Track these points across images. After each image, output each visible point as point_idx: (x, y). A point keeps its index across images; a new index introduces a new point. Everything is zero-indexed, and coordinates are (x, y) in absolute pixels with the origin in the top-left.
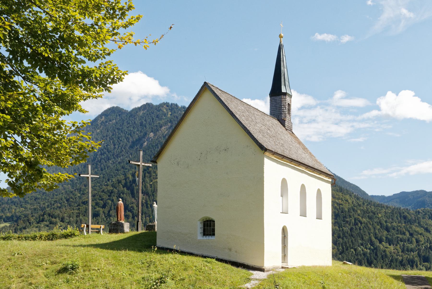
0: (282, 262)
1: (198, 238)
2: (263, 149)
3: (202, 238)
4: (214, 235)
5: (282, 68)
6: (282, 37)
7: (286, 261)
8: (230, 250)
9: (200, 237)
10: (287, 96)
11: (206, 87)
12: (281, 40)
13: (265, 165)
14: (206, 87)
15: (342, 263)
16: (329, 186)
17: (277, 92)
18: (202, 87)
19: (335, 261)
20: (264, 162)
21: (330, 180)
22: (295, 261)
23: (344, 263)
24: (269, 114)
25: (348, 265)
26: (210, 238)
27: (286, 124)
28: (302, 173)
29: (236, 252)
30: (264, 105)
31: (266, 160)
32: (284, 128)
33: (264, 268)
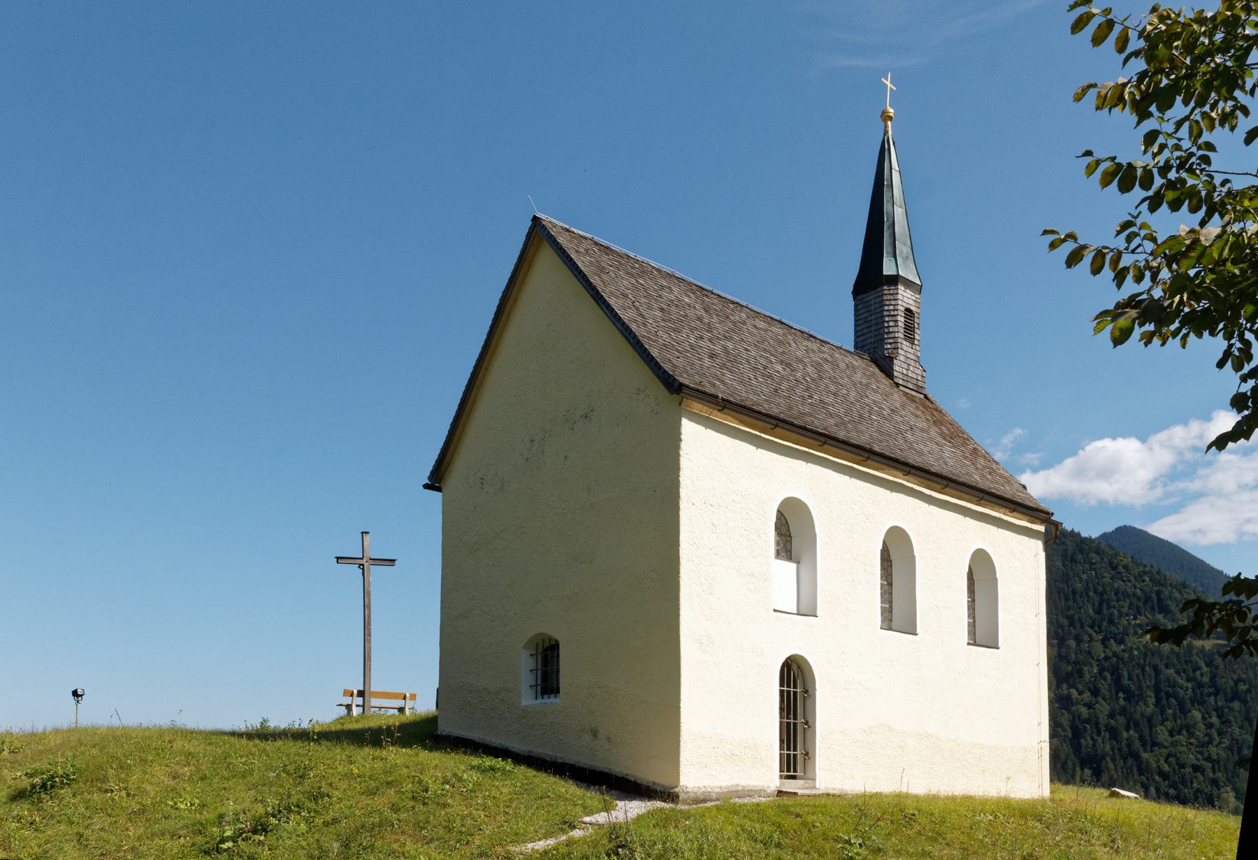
0: (781, 777)
1: (524, 703)
2: (673, 386)
3: (534, 702)
4: (558, 692)
5: (887, 207)
6: (891, 118)
7: (809, 774)
8: (595, 734)
9: (527, 699)
10: (901, 287)
11: (538, 233)
12: (886, 126)
13: (683, 445)
14: (538, 233)
15: (1106, 793)
16: (1037, 547)
17: (871, 281)
18: (529, 236)
19: (1058, 785)
20: (680, 434)
21: (1041, 528)
22: (839, 769)
23: (1114, 794)
24: (852, 349)
25: (1125, 800)
26: (553, 699)
27: (896, 368)
28: (892, 490)
29: (609, 740)
30: (839, 323)
31: (689, 429)
32: (886, 381)
33: (677, 790)
